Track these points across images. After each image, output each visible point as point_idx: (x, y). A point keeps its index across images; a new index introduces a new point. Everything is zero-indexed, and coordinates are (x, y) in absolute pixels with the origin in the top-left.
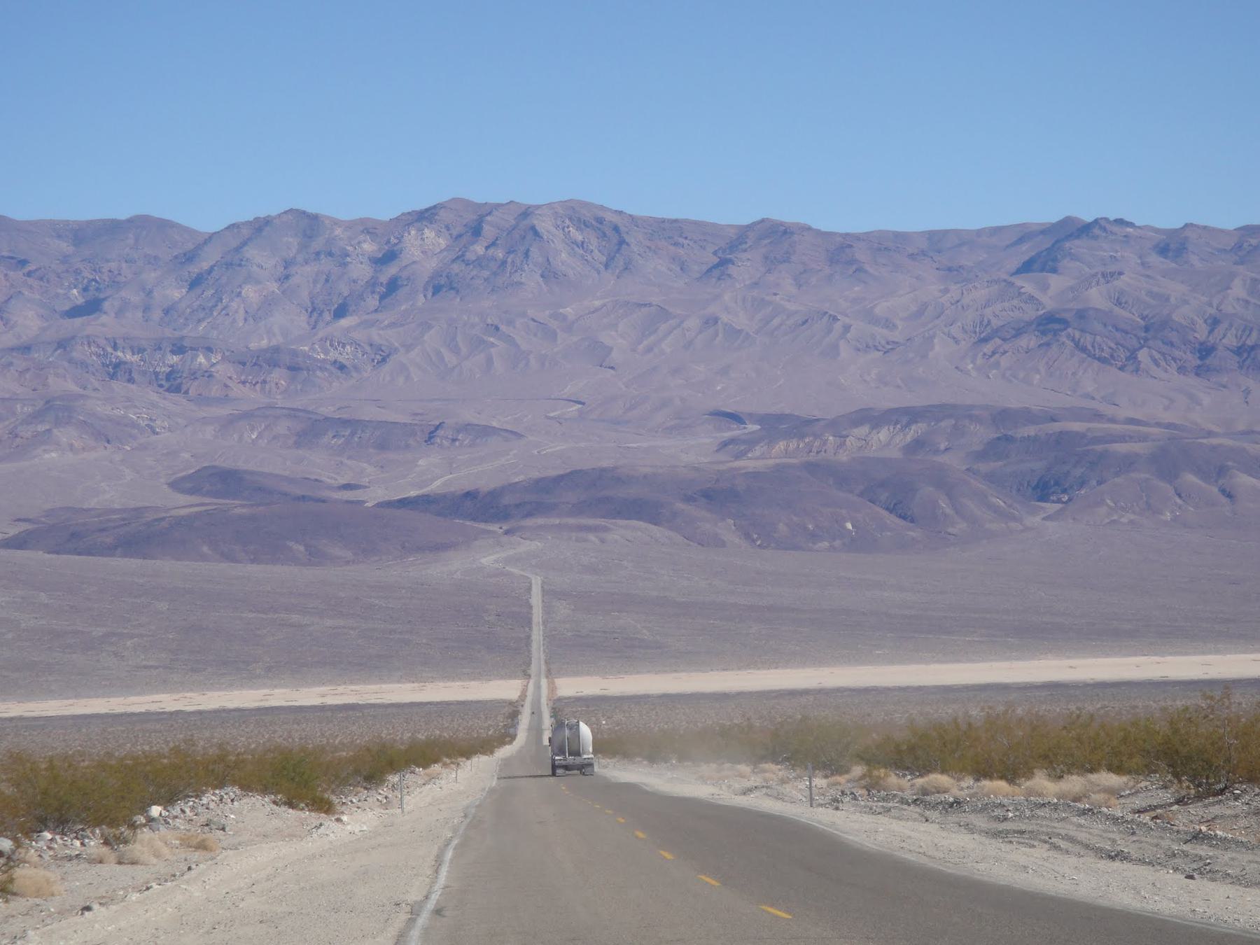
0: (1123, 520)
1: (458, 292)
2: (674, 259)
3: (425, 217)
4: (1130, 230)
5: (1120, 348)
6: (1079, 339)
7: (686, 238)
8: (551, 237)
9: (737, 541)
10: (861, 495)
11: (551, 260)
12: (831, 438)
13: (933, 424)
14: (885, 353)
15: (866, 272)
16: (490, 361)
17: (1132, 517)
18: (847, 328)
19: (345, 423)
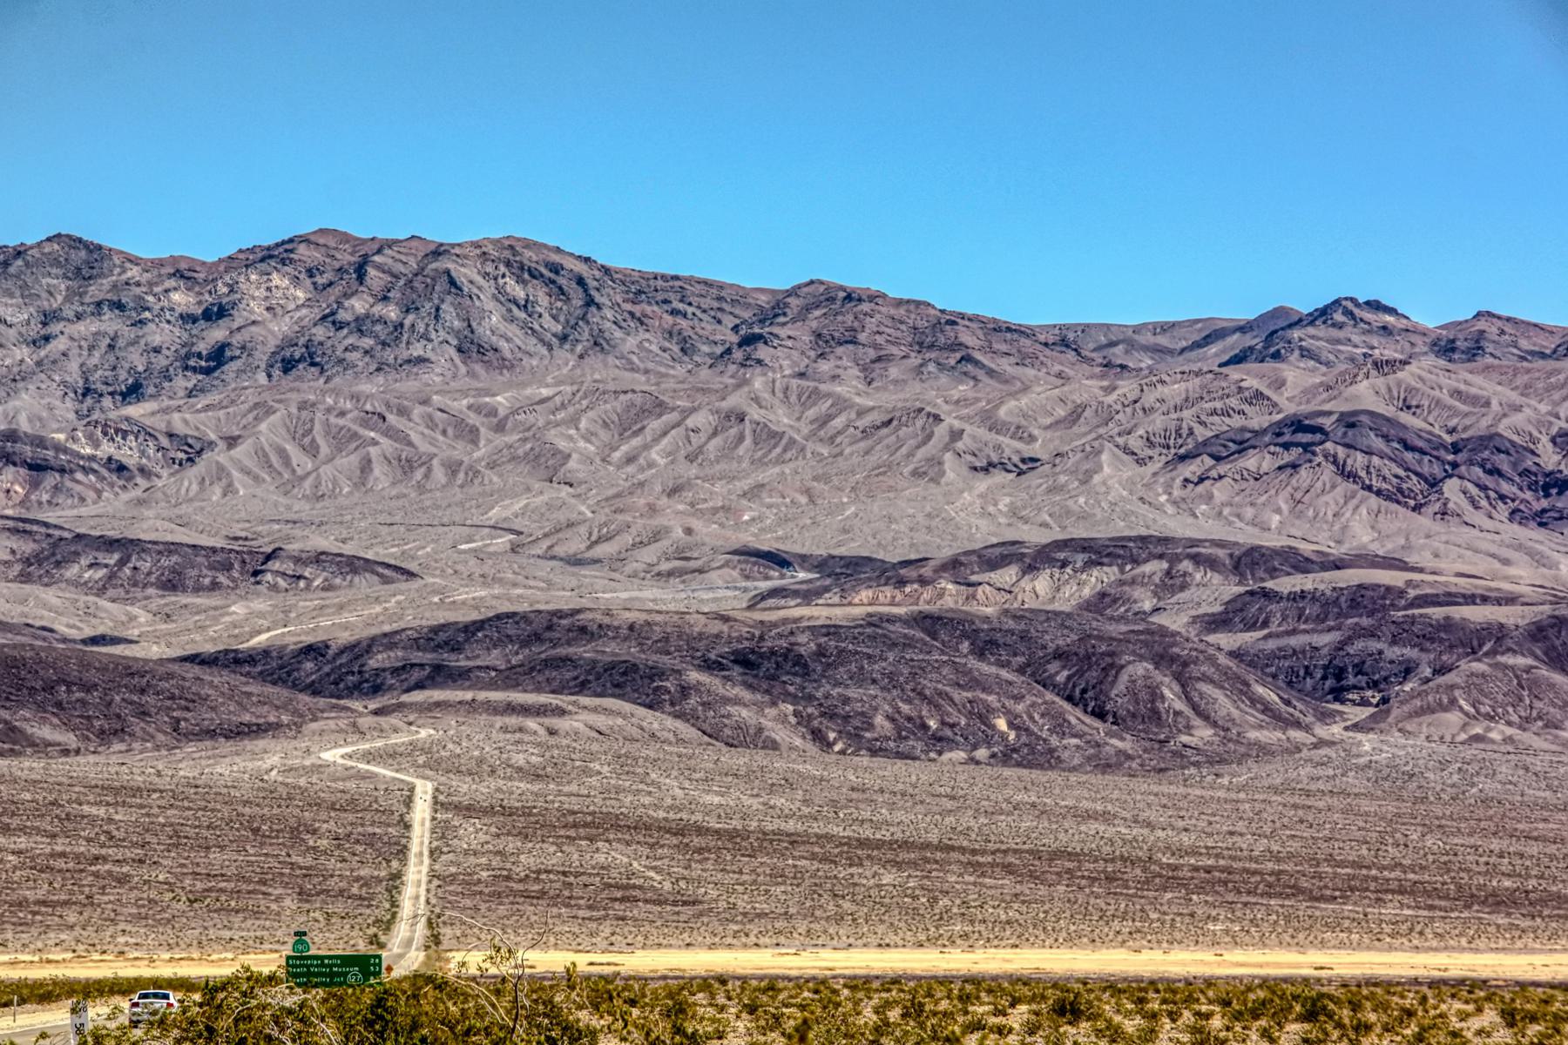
0: (1494, 735)
1: (322, 371)
2: (670, 334)
3: (276, 255)
4: (1389, 319)
5: (1413, 477)
6: (1345, 462)
7: (690, 304)
8: (475, 290)
9: (798, 742)
10: (1021, 670)
11: (474, 324)
12: (950, 586)
13: (1128, 567)
14: (1019, 474)
15: (977, 363)
16: (366, 466)
17: (1509, 731)
18: (956, 435)
19: (110, 544)
